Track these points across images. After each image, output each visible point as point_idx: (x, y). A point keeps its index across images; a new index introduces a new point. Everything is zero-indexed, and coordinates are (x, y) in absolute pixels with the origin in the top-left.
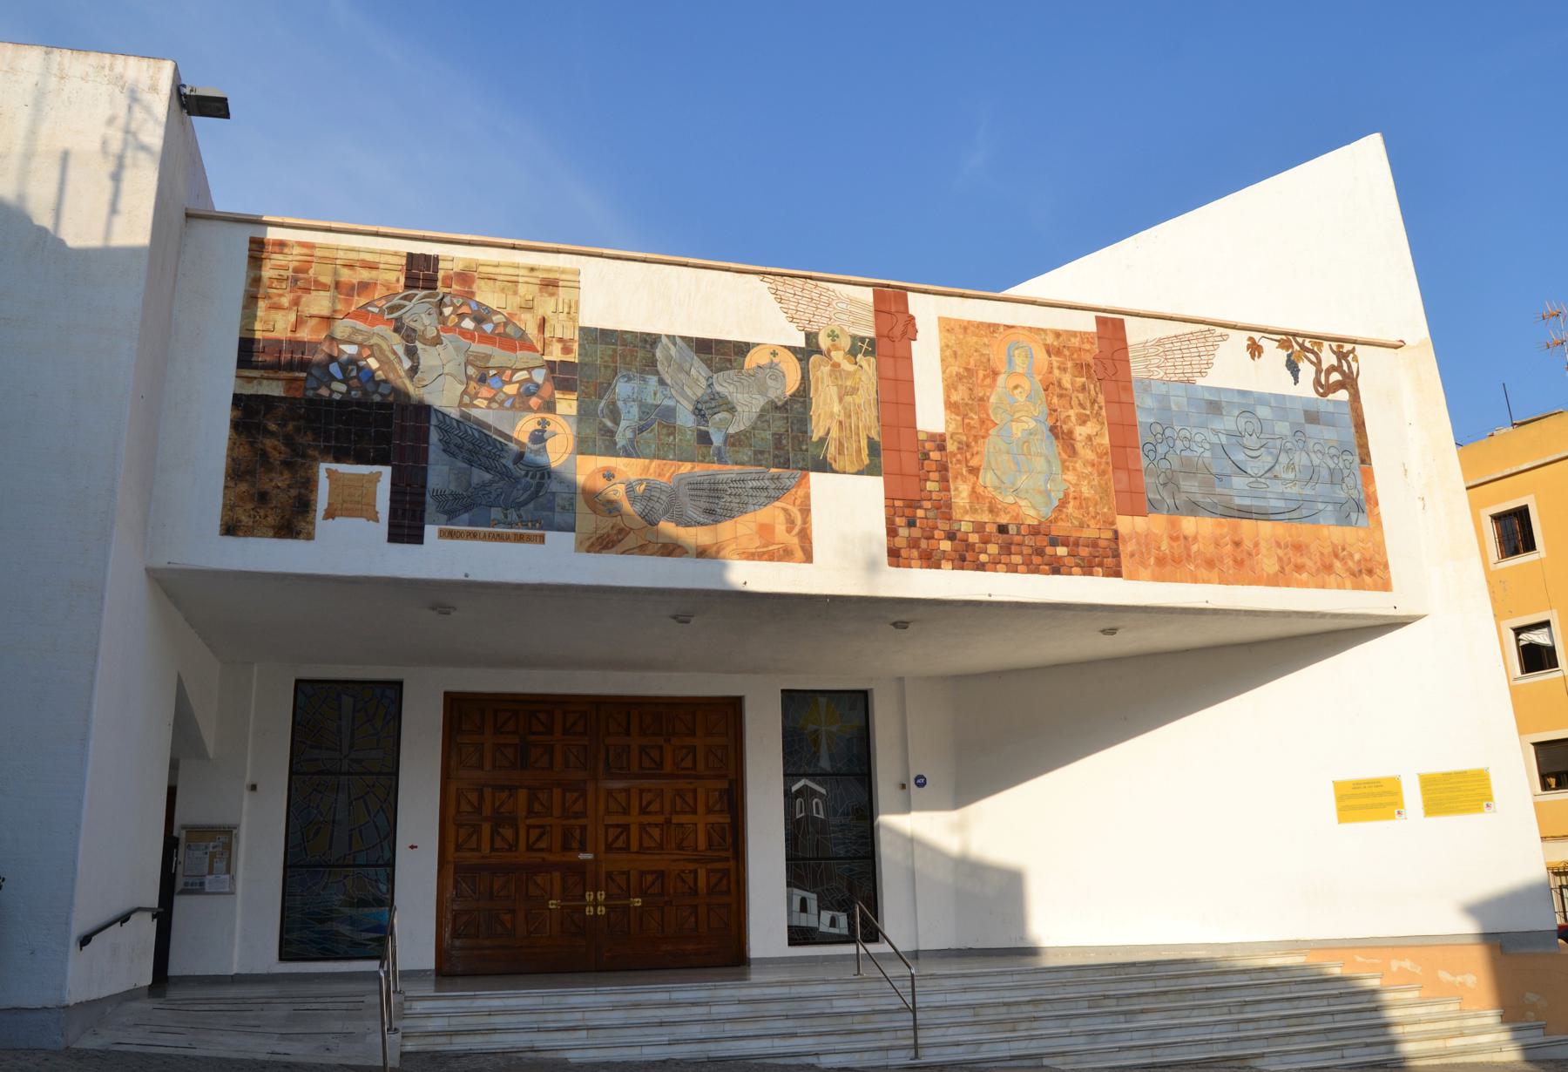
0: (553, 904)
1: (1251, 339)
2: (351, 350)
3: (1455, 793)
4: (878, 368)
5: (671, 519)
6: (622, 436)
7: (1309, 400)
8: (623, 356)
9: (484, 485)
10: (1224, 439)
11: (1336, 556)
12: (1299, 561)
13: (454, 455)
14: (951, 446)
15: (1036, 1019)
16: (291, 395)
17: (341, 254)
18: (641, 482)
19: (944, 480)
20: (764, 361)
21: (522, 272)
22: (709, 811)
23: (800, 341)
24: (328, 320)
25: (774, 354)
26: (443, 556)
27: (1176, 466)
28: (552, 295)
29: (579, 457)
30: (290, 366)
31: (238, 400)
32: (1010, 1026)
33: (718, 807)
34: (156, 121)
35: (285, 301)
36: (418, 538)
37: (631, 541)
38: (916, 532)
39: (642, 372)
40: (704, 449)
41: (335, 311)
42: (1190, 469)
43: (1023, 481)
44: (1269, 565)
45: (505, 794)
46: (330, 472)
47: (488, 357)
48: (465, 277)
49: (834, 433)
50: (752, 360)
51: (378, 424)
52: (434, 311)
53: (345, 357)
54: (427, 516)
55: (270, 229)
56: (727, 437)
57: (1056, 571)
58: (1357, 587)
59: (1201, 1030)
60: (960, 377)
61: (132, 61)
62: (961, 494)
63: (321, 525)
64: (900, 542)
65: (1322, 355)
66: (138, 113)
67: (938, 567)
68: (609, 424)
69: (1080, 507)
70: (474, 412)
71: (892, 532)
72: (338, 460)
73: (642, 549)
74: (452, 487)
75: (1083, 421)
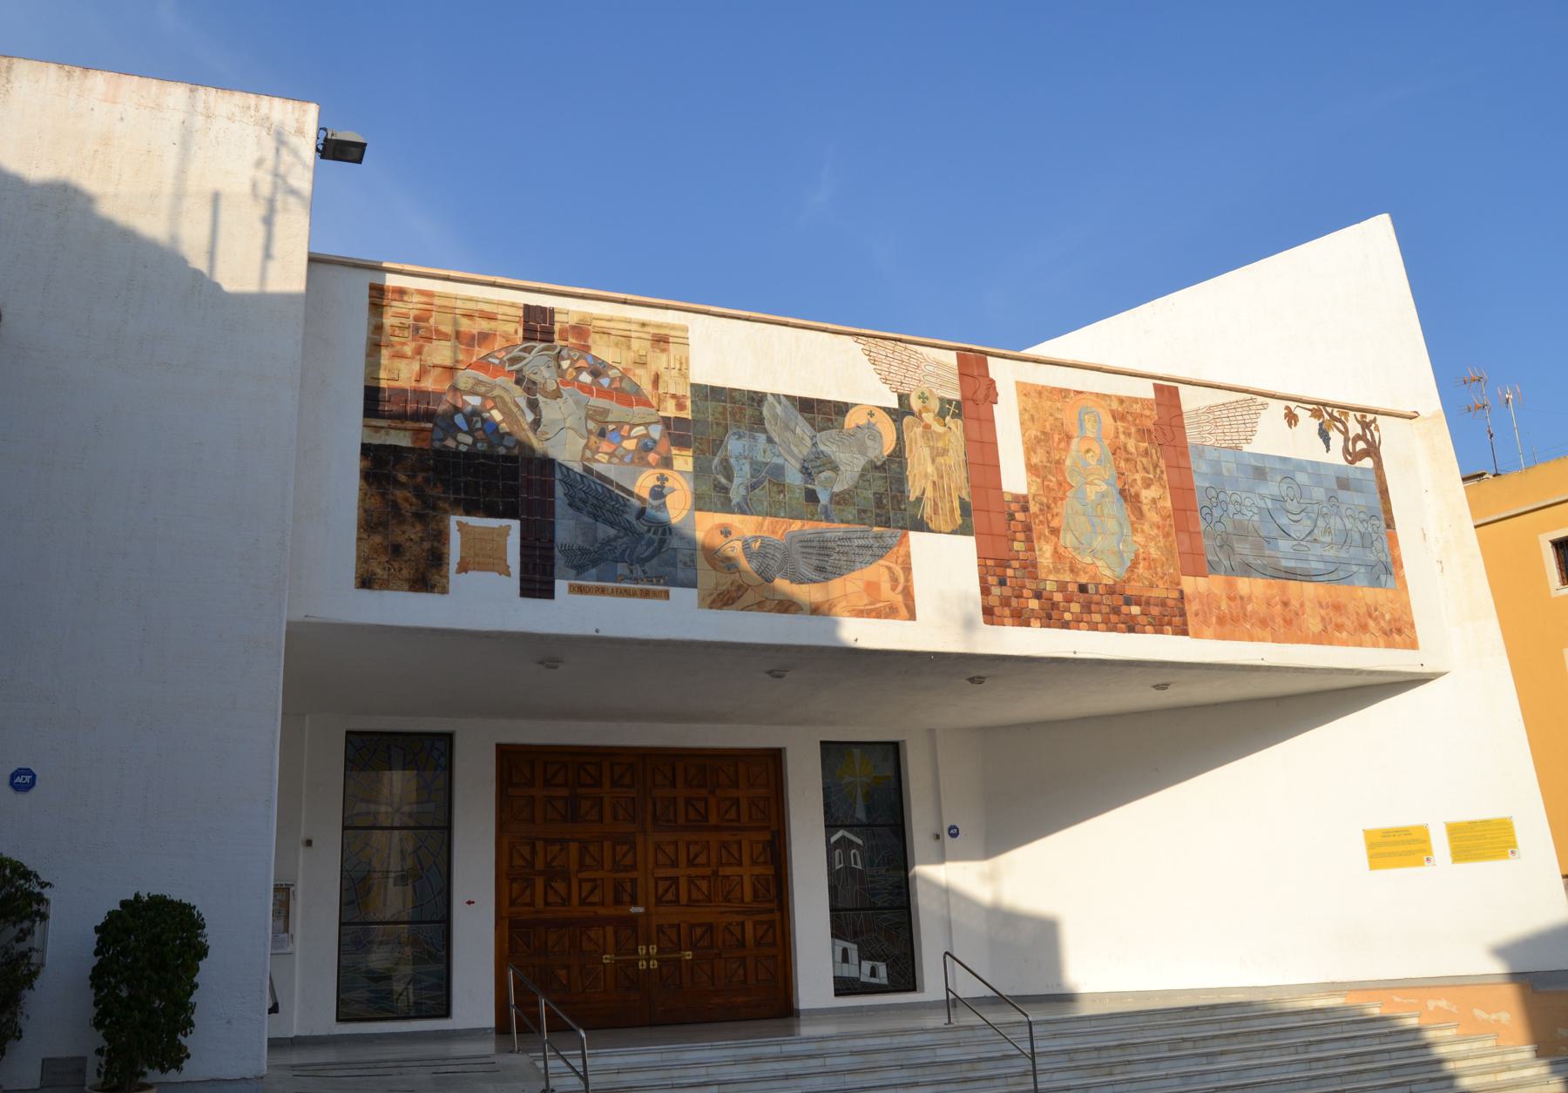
0: (607, 959)
1: (1287, 408)
2: (474, 401)
3: (1481, 840)
4: (965, 430)
5: (785, 576)
6: (737, 493)
7: (1339, 466)
8: (733, 414)
9: (609, 541)
10: (1269, 504)
11: (1370, 615)
12: (1339, 621)
13: (579, 509)
14: (1034, 508)
15: (1130, 1062)
16: (417, 446)
17: (459, 304)
18: (756, 538)
19: (1029, 540)
20: (863, 421)
21: (633, 327)
22: (754, 863)
23: (895, 404)
24: (451, 370)
25: (871, 414)
26: (574, 611)
27: (1230, 530)
28: (664, 350)
29: (697, 514)
30: (416, 416)
31: (366, 449)
32: (1107, 1070)
33: (762, 859)
34: (304, 165)
35: (408, 350)
36: (549, 593)
37: (749, 597)
38: (1007, 591)
39: (751, 430)
40: (811, 508)
41: (457, 362)
42: (1242, 532)
43: (1098, 543)
44: (1314, 625)
45: (557, 848)
46: (461, 525)
47: (606, 412)
48: (580, 330)
49: (929, 493)
50: (852, 420)
51: (504, 477)
52: (553, 363)
53: (469, 409)
54: (556, 570)
55: (388, 276)
56: (833, 496)
57: (1131, 630)
58: (1389, 645)
59: (1278, 1070)
60: (1039, 441)
61: (277, 102)
62: (1045, 554)
63: (455, 579)
64: (993, 601)
65: (1349, 425)
66: (286, 157)
67: (1028, 625)
68: (723, 481)
69: (1149, 568)
70: (596, 467)
71: (985, 590)
72: (468, 513)
73: (760, 606)
74: (580, 542)
75: (1148, 484)
